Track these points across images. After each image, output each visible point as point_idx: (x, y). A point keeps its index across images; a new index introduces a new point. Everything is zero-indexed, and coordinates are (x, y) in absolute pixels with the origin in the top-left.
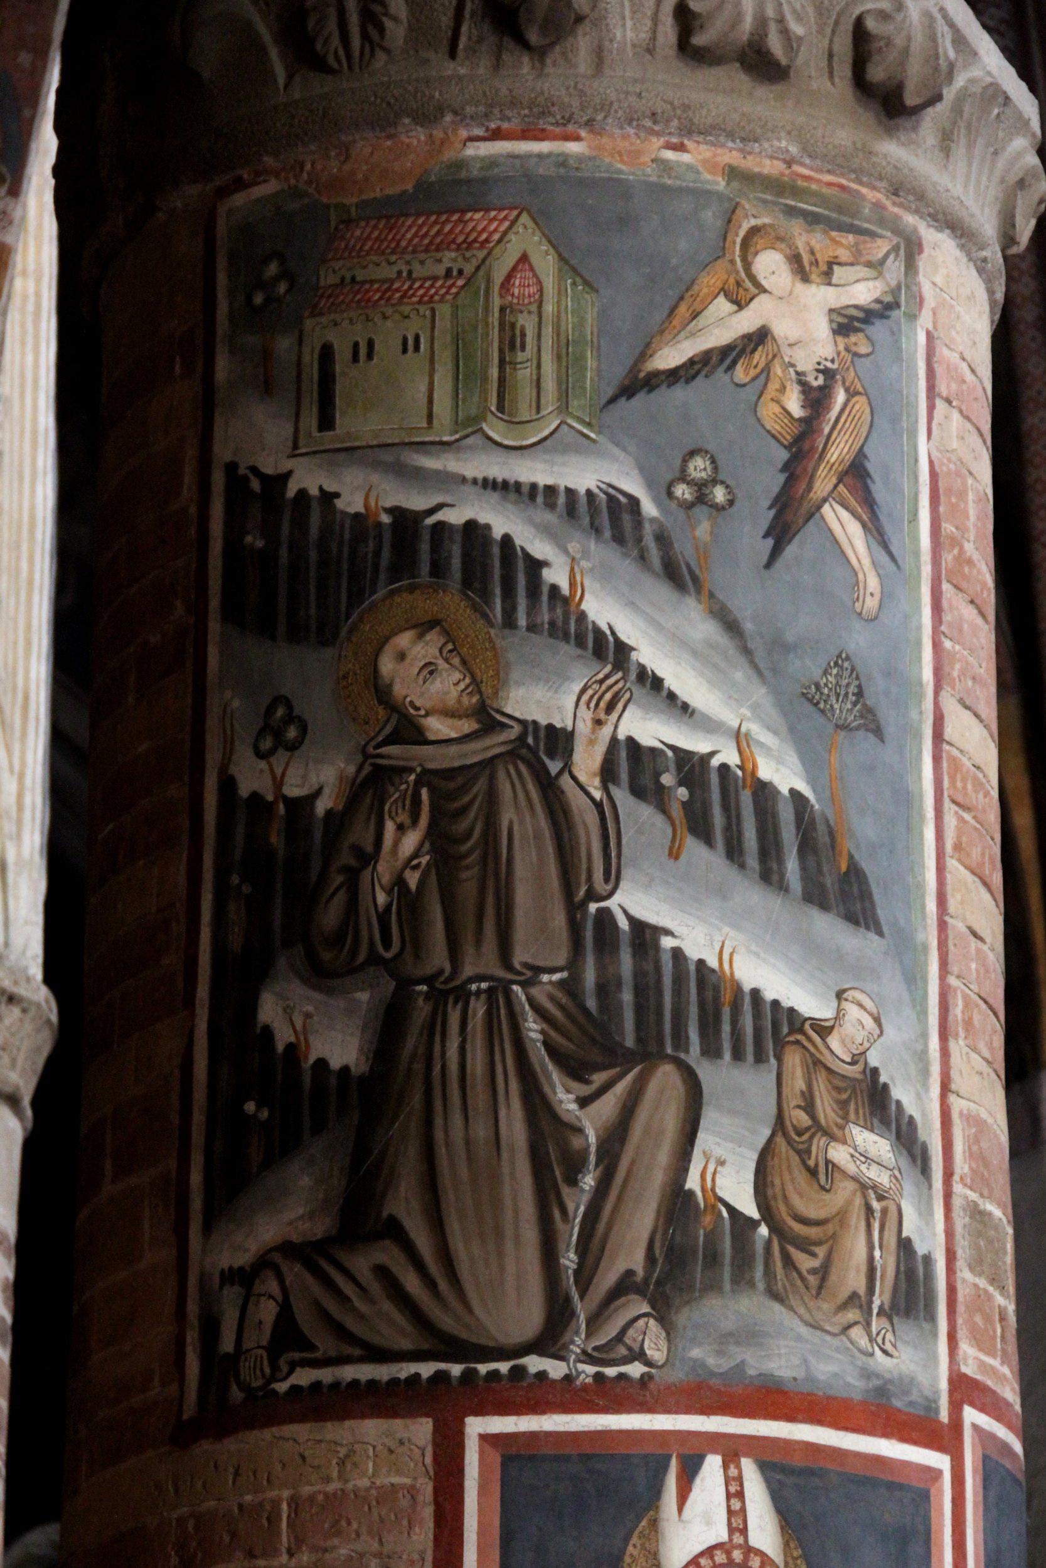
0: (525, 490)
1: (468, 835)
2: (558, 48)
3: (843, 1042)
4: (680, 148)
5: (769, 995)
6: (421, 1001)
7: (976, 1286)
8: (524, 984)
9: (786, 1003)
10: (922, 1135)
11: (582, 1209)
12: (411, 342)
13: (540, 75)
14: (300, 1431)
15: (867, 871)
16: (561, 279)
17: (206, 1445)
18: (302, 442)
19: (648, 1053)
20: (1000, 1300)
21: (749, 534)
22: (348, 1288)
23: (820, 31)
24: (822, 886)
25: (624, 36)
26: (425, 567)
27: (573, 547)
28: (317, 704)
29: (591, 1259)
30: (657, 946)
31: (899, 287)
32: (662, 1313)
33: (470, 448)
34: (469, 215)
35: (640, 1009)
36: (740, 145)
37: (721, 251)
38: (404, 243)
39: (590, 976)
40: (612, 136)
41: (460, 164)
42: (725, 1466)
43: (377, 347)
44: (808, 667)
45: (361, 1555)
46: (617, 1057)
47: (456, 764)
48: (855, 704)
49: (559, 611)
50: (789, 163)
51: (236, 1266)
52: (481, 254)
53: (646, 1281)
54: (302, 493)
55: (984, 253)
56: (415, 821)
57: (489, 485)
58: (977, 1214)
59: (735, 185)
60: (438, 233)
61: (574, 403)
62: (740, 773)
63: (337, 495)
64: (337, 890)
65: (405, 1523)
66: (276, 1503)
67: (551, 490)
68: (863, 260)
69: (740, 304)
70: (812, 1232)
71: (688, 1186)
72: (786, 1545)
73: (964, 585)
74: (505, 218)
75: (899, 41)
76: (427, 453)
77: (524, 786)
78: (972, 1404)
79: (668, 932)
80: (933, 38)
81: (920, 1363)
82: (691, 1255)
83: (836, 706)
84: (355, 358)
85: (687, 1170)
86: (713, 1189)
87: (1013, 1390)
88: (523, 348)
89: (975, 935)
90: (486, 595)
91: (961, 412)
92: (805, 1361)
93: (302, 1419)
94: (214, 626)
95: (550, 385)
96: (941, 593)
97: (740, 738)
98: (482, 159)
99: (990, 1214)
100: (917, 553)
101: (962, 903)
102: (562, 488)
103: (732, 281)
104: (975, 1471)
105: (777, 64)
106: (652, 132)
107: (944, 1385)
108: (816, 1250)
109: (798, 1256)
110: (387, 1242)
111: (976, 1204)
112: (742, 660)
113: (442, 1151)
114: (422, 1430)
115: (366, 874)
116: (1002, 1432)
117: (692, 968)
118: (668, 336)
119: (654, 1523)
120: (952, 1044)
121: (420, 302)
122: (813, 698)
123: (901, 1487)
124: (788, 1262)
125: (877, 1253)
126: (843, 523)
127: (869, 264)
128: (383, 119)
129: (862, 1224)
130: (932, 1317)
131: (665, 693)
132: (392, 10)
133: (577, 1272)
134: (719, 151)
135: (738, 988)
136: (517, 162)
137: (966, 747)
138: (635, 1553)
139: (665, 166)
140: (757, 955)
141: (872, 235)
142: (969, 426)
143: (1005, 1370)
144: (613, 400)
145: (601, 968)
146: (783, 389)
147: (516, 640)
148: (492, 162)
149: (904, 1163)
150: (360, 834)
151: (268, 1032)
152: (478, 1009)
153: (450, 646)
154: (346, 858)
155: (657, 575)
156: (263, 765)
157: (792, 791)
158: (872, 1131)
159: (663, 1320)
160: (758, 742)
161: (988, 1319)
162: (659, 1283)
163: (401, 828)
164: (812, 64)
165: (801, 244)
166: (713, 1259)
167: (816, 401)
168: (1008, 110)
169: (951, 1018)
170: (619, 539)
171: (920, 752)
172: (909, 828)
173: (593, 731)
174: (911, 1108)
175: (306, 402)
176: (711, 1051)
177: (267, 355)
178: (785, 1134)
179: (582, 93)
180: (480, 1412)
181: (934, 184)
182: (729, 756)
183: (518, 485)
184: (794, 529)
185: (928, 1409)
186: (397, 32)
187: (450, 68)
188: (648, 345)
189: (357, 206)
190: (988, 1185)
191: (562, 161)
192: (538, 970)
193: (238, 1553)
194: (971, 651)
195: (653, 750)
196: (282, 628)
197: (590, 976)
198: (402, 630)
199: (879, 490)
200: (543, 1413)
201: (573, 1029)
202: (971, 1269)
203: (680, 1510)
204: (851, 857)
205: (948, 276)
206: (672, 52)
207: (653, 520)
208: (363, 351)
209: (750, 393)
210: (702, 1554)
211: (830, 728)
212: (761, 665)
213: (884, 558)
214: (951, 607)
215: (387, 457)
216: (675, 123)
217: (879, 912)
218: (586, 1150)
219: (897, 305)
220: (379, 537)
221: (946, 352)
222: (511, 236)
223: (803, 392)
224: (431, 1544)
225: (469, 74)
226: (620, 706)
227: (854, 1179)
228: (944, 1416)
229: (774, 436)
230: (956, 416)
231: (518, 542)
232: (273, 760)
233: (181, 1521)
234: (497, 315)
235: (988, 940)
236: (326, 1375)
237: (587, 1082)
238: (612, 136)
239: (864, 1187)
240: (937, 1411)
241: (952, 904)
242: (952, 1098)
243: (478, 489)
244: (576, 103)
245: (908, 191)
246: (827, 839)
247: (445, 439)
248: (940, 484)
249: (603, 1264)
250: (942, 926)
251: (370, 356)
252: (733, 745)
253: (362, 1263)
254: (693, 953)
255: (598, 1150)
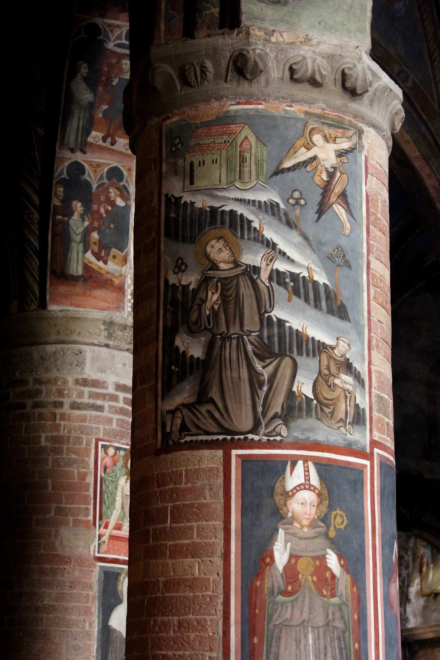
0: (247, 201)
1: (231, 296)
2: (255, 79)
3: (339, 352)
4: (291, 106)
5: (317, 339)
6: (219, 340)
7: (379, 416)
8: (247, 336)
9: (322, 341)
10: (362, 376)
11: (263, 396)
12: (215, 161)
13: (251, 87)
14: (188, 452)
15: (346, 305)
16: (256, 142)
17: (163, 456)
18: (185, 188)
19: (282, 354)
20: (387, 420)
21: (311, 213)
22: (200, 416)
23: (332, 73)
24: (332, 309)
25: (274, 76)
26: (219, 222)
27: (260, 217)
28: (190, 260)
29: (266, 409)
30: (284, 326)
31: (356, 144)
32: (286, 423)
33: (231, 190)
34: (231, 126)
35: (280, 342)
36: (308, 105)
37: (303, 135)
38: (213, 134)
39: (265, 334)
40: (271, 103)
41: (228, 112)
42: (304, 464)
43: (205, 162)
44: (328, 249)
45: (204, 485)
46: (273, 355)
47: (228, 276)
48: (342, 259)
49: (256, 234)
50: (323, 110)
51: (170, 409)
52: (234, 136)
53: (281, 415)
54: (185, 202)
55: (384, 133)
56: (217, 292)
57: (237, 200)
58: (380, 398)
59: (307, 116)
60: (222, 131)
61: (260, 177)
62: (308, 278)
63: (195, 203)
64: (196, 310)
65: (216, 477)
66: (182, 471)
67: (254, 201)
68: (345, 136)
69: (308, 149)
70: (329, 402)
71: (293, 390)
72: (321, 484)
73: (377, 226)
74: (241, 126)
75: (355, 76)
76: (219, 191)
77: (247, 282)
78: (377, 448)
79: (288, 322)
80: (365, 74)
81: (361, 437)
82: (294, 408)
83: (337, 260)
84: (200, 165)
85: (293, 386)
86: (300, 391)
87: (391, 444)
88: (246, 162)
89: (380, 322)
90: (236, 230)
91: (376, 177)
92: (327, 436)
93: (188, 449)
94: (163, 238)
95: (253, 172)
96: (369, 228)
97: (308, 269)
98: (234, 110)
99: (384, 397)
100: (362, 217)
101: (376, 313)
102: (257, 201)
103: (306, 143)
104: (377, 465)
105: (319, 83)
106: (282, 102)
107: (368, 443)
108: (330, 407)
109: (325, 408)
110: (210, 404)
111: (379, 395)
112: (309, 248)
113: (224, 380)
114: (220, 453)
115: (203, 306)
116: (386, 455)
117: (295, 331)
118: (287, 158)
119: (284, 478)
120: (372, 352)
121: (217, 150)
122: (330, 258)
123: (355, 469)
124: (322, 410)
125: (348, 408)
126: (339, 210)
127: (347, 138)
128: (207, 100)
129: (344, 400)
130: (364, 424)
131: (286, 257)
132: (209, 70)
133: (262, 413)
134: (302, 107)
135: (308, 337)
136: (244, 111)
137: (379, 271)
138: (279, 486)
139: (287, 112)
140: (313, 328)
141: (348, 129)
142: (379, 181)
143: (389, 439)
144: (271, 176)
145: (268, 331)
146: (321, 173)
147: (244, 242)
148: (237, 111)
149: (357, 383)
150: (202, 295)
151: (177, 348)
152: (234, 342)
153: (226, 244)
154: (198, 301)
155: (284, 224)
156: (175, 276)
157: (324, 284)
158: (347, 375)
159: (287, 425)
160: (314, 270)
161: (382, 425)
162: (285, 415)
163: (213, 293)
164: (330, 83)
165: (326, 132)
166: (300, 409)
167: (331, 175)
168: (392, 93)
169: (372, 345)
170: (273, 214)
171: (362, 273)
172: (359, 293)
173: (266, 267)
174: (359, 369)
175: (186, 177)
176: (300, 353)
177: (176, 164)
178: (321, 376)
179: (262, 92)
180: (236, 448)
181: (367, 115)
182: (305, 274)
183: (245, 200)
184: (324, 211)
185: (363, 449)
186: (210, 76)
187: (225, 85)
188: (282, 161)
189: (200, 123)
190: (383, 389)
191: (257, 110)
192: (251, 332)
193: (172, 483)
194: (380, 244)
195: (283, 272)
196: (180, 239)
197: (265, 334)
198: (213, 240)
199: (350, 200)
200: (253, 449)
201: (261, 348)
202: (378, 412)
203: (291, 474)
204: (341, 301)
205: (372, 140)
206: (289, 80)
207: (283, 209)
208: (202, 163)
209: (311, 174)
210: (297, 486)
211: (335, 265)
212: (315, 249)
213: (352, 219)
214: (373, 232)
215: (208, 192)
216: (289, 99)
217: (350, 316)
218: (264, 381)
219: (356, 149)
220: (206, 214)
221: (371, 161)
222: (243, 131)
223: (327, 173)
224: (222, 482)
225: (230, 87)
226: (274, 260)
227: (341, 388)
228: (368, 451)
229: (319, 186)
230: (375, 179)
231: (245, 215)
232: (179, 275)
233: (157, 475)
234: (238, 153)
235: (385, 323)
236: (194, 438)
237: (265, 362)
238: (271, 103)
239: (344, 390)
240: (366, 450)
241: (372, 314)
242: (372, 366)
243: (234, 201)
244: (260, 94)
245: (359, 117)
246: (334, 296)
247: (224, 187)
248: (369, 198)
249: (269, 411)
250: (369, 320)
251: (204, 164)
252: (306, 271)
253: (203, 409)
254: (295, 327)
255: (268, 380)
